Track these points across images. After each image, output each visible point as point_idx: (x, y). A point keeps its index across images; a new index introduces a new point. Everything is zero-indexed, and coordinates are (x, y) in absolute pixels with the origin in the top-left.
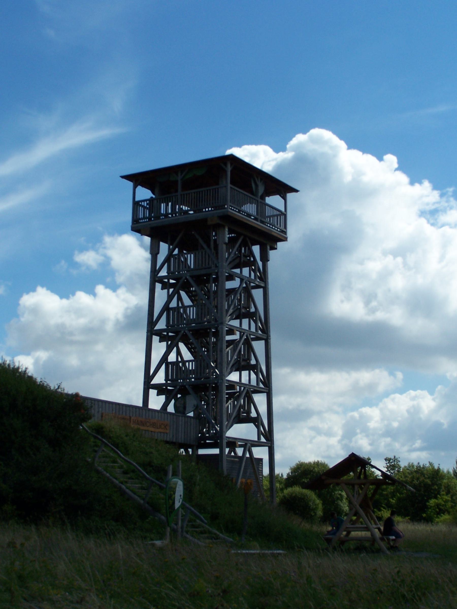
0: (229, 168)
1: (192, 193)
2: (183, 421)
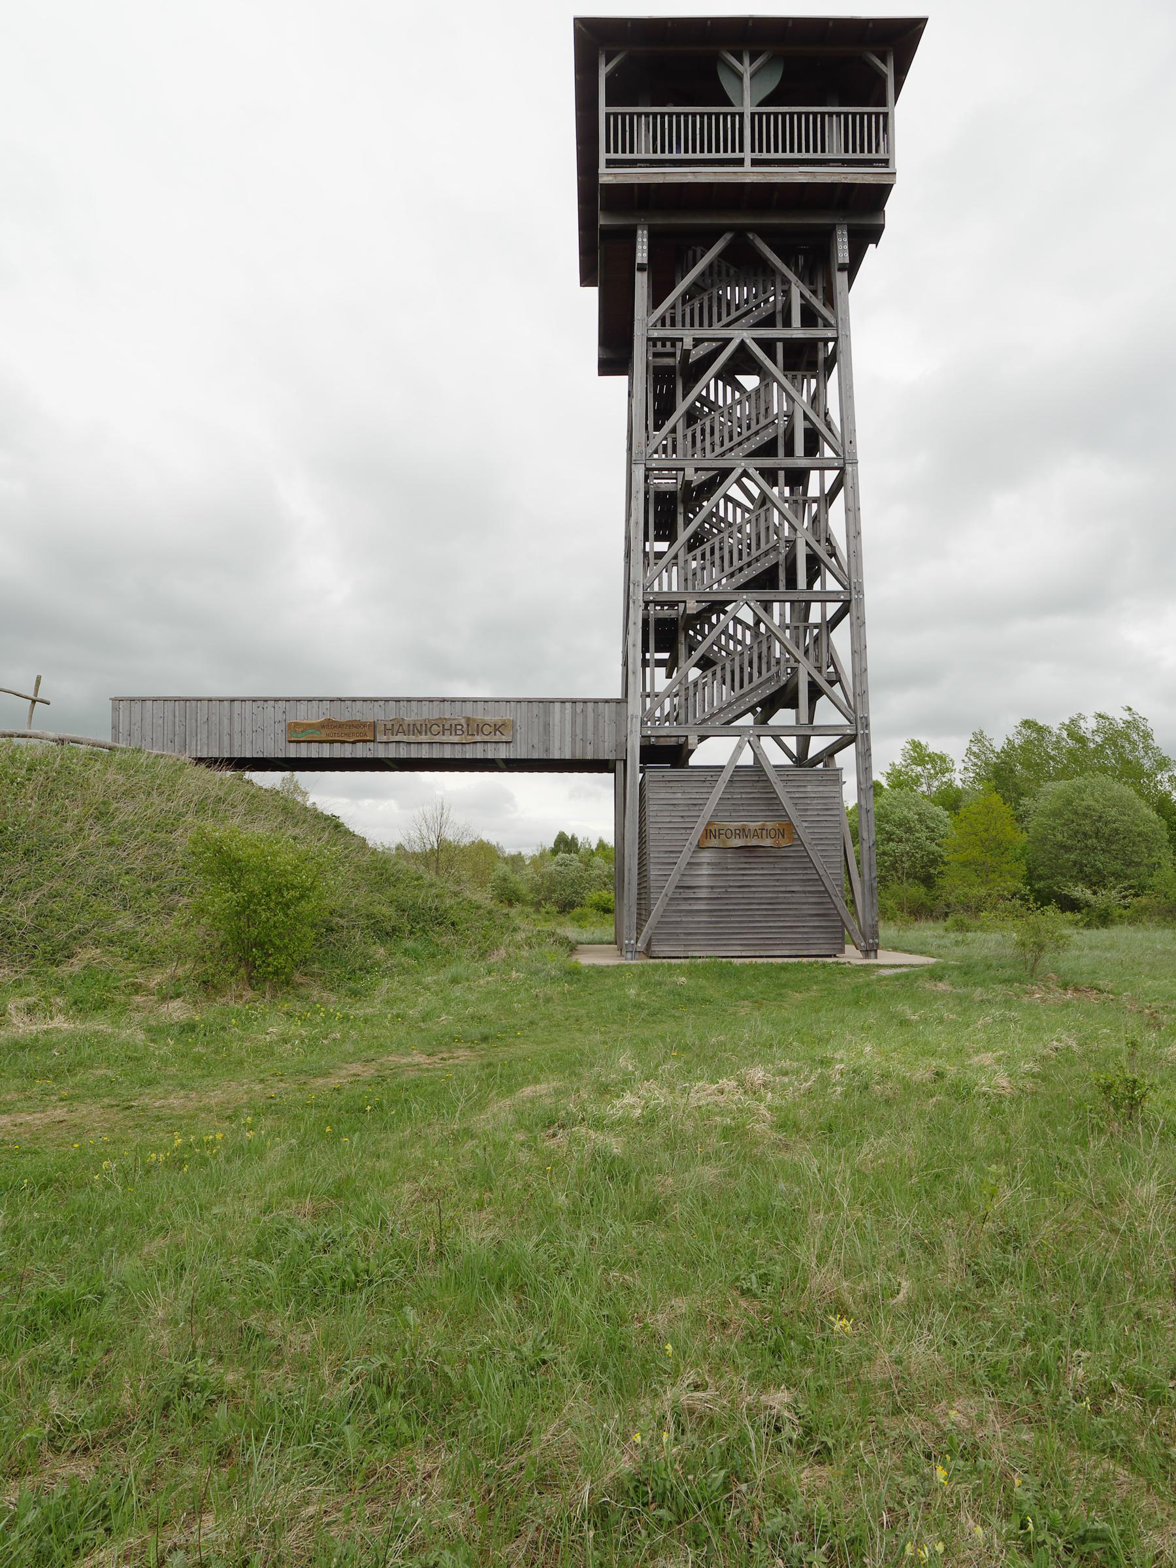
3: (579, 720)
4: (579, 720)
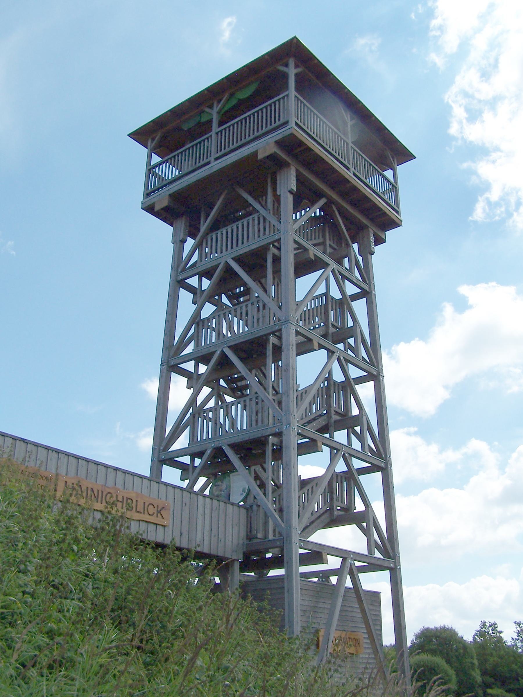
0: (292, 71)
1: (233, 125)
2: (208, 506)
3: (215, 514)
4: (215, 514)
